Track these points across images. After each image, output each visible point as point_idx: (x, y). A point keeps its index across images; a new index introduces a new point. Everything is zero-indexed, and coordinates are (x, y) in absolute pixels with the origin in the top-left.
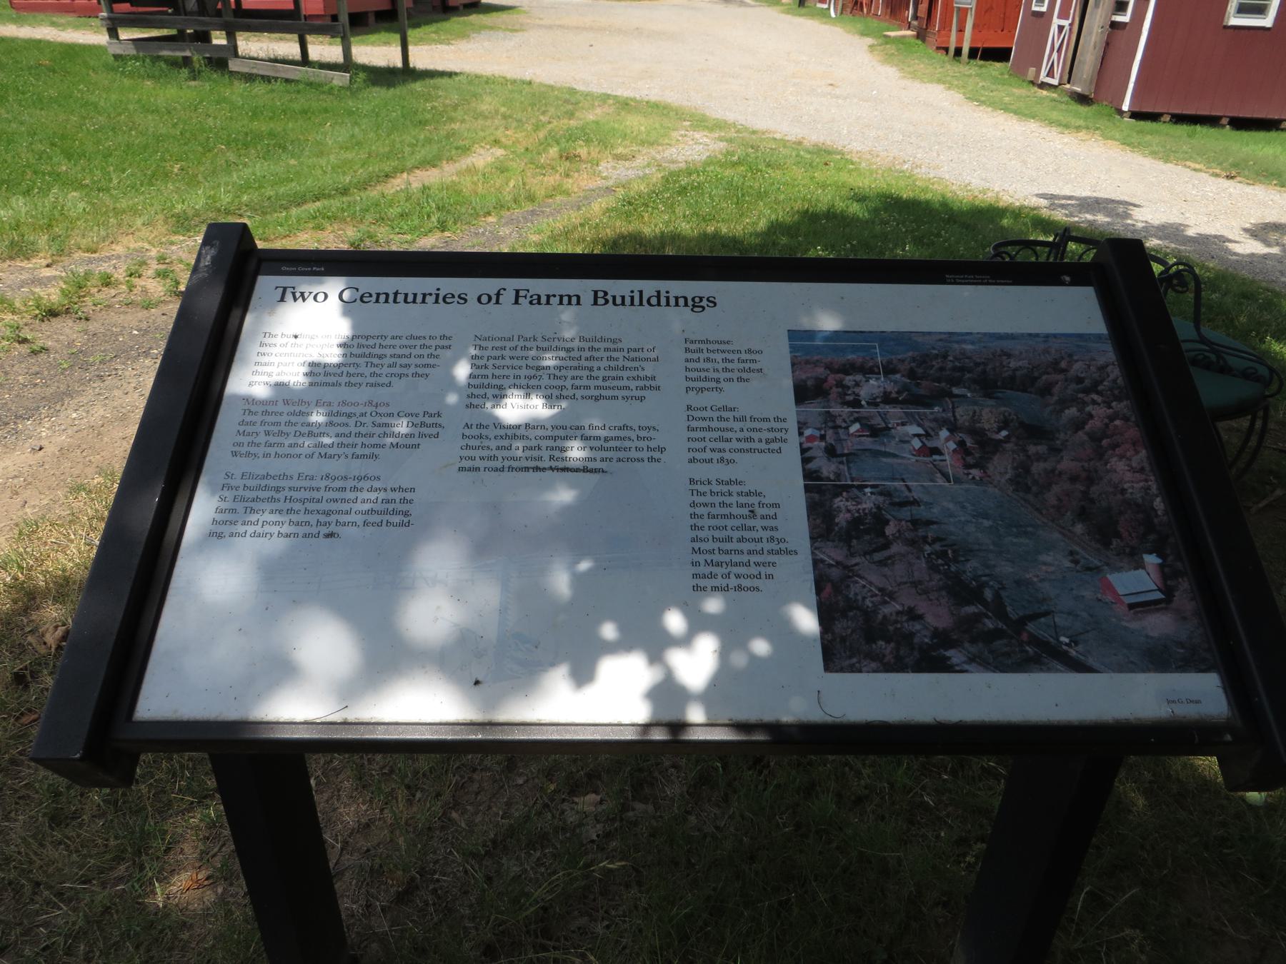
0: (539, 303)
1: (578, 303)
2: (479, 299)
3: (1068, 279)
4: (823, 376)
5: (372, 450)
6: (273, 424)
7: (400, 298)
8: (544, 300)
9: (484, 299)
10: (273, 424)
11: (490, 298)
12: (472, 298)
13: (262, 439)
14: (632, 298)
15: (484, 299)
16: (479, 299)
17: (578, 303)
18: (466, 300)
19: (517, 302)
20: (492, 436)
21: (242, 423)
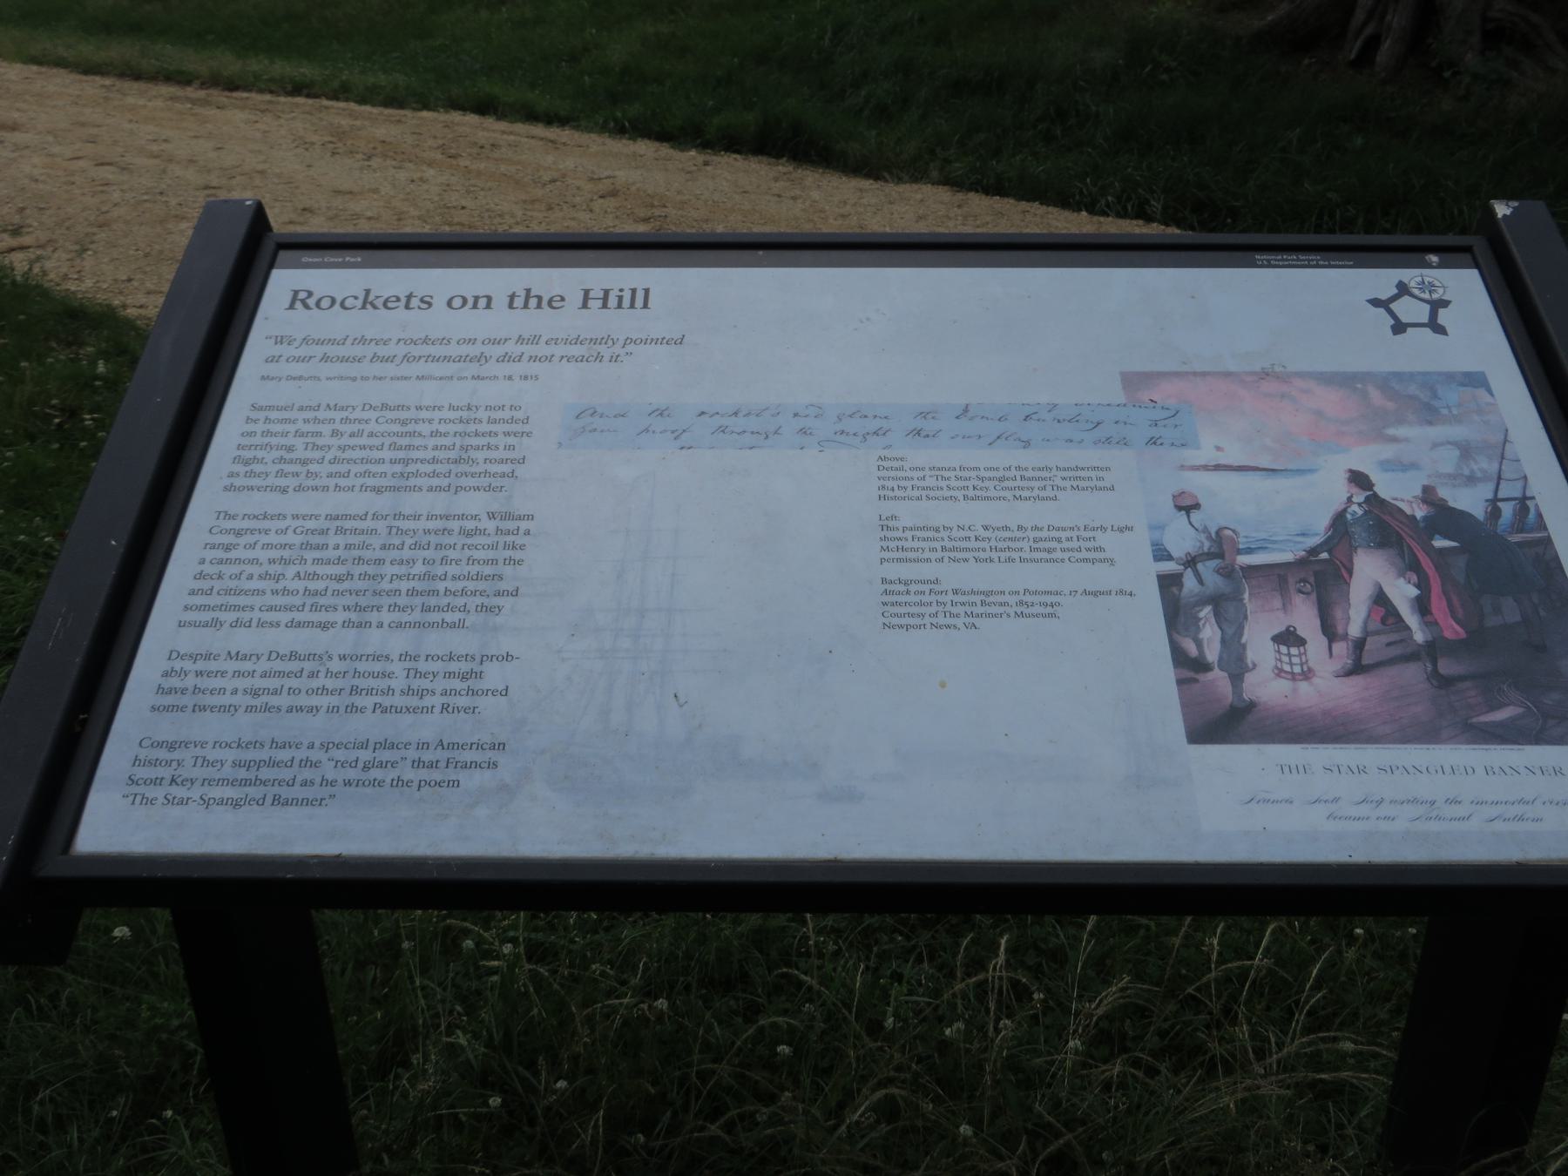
1: (488, 306)
2: (449, 304)
4: (115, 334)
5: (362, 538)
6: (486, 562)
7: (415, 302)
9: (457, 302)
10: (486, 562)
11: (465, 301)
12: (500, 301)
13: (397, 668)
14: (620, 298)
15: (457, 302)
16: (449, 304)
17: (488, 306)
18: (430, 304)
19: (585, 306)
20: (501, 436)
21: (201, 576)
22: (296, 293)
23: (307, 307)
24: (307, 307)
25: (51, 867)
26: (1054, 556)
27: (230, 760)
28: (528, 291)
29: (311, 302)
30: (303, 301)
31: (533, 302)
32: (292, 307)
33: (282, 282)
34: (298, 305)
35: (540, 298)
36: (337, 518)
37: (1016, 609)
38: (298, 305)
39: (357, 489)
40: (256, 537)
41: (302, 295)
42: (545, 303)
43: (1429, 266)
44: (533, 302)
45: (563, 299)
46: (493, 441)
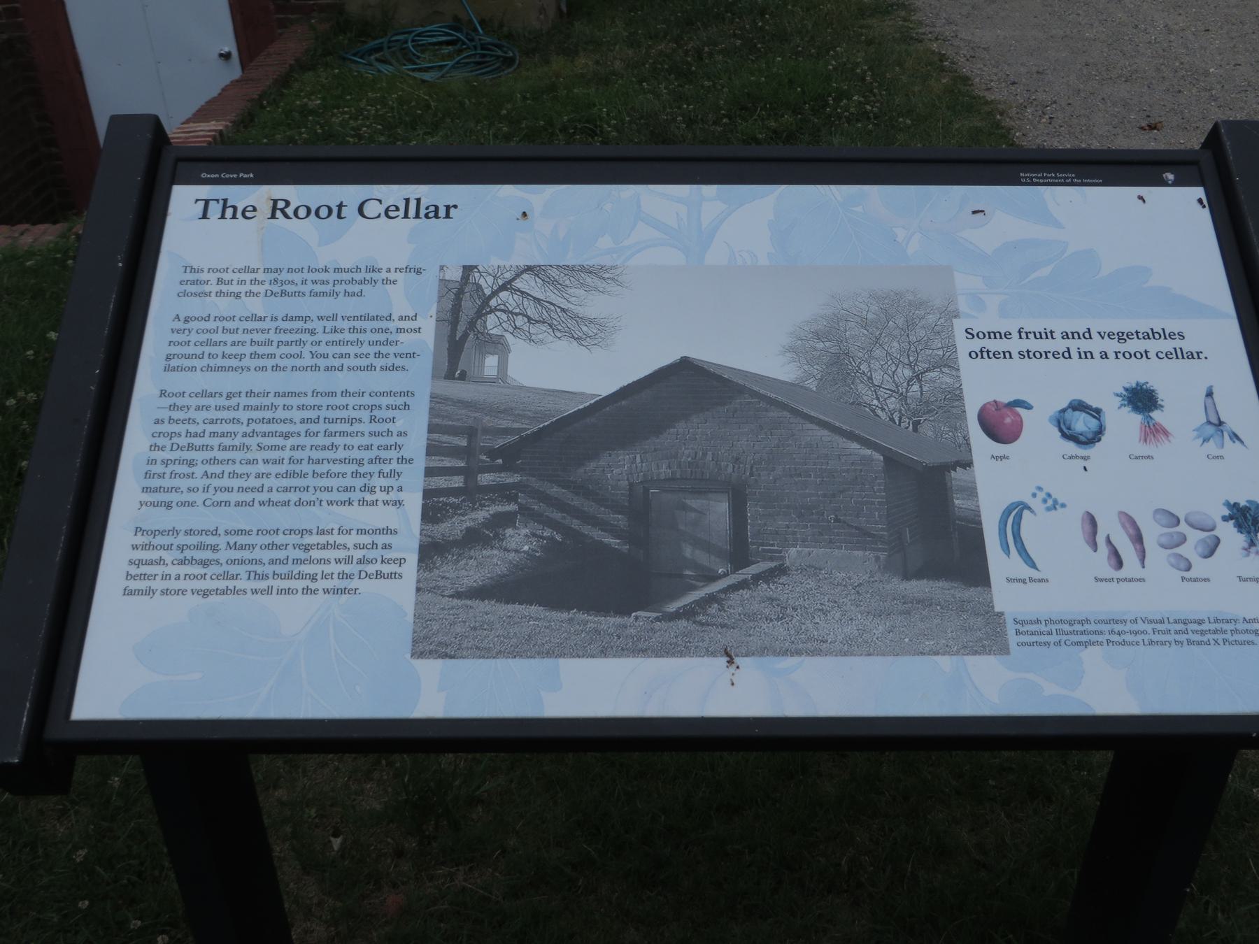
0: (436, 216)
3: (1170, 177)
8: (442, 213)
22: (275, 202)
23: (287, 216)
24: (287, 216)
25: (54, 732)
26: (267, 540)
27: (160, 573)
28: (225, 201)
29: (290, 211)
30: (282, 210)
31: (229, 212)
32: (273, 216)
33: (184, 200)
34: (278, 214)
35: (235, 208)
36: (284, 395)
37: (1108, 636)
38: (278, 214)
39: (269, 369)
40: (227, 403)
41: (281, 205)
42: (239, 214)
43: (1164, 183)
44: (229, 212)
45: (255, 209)
46: (362, 337)
